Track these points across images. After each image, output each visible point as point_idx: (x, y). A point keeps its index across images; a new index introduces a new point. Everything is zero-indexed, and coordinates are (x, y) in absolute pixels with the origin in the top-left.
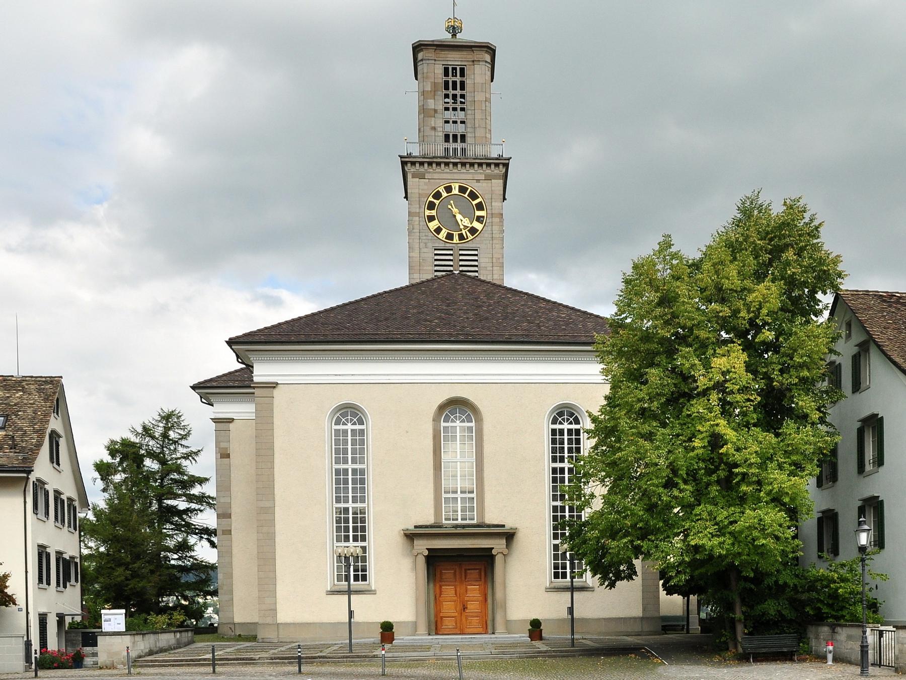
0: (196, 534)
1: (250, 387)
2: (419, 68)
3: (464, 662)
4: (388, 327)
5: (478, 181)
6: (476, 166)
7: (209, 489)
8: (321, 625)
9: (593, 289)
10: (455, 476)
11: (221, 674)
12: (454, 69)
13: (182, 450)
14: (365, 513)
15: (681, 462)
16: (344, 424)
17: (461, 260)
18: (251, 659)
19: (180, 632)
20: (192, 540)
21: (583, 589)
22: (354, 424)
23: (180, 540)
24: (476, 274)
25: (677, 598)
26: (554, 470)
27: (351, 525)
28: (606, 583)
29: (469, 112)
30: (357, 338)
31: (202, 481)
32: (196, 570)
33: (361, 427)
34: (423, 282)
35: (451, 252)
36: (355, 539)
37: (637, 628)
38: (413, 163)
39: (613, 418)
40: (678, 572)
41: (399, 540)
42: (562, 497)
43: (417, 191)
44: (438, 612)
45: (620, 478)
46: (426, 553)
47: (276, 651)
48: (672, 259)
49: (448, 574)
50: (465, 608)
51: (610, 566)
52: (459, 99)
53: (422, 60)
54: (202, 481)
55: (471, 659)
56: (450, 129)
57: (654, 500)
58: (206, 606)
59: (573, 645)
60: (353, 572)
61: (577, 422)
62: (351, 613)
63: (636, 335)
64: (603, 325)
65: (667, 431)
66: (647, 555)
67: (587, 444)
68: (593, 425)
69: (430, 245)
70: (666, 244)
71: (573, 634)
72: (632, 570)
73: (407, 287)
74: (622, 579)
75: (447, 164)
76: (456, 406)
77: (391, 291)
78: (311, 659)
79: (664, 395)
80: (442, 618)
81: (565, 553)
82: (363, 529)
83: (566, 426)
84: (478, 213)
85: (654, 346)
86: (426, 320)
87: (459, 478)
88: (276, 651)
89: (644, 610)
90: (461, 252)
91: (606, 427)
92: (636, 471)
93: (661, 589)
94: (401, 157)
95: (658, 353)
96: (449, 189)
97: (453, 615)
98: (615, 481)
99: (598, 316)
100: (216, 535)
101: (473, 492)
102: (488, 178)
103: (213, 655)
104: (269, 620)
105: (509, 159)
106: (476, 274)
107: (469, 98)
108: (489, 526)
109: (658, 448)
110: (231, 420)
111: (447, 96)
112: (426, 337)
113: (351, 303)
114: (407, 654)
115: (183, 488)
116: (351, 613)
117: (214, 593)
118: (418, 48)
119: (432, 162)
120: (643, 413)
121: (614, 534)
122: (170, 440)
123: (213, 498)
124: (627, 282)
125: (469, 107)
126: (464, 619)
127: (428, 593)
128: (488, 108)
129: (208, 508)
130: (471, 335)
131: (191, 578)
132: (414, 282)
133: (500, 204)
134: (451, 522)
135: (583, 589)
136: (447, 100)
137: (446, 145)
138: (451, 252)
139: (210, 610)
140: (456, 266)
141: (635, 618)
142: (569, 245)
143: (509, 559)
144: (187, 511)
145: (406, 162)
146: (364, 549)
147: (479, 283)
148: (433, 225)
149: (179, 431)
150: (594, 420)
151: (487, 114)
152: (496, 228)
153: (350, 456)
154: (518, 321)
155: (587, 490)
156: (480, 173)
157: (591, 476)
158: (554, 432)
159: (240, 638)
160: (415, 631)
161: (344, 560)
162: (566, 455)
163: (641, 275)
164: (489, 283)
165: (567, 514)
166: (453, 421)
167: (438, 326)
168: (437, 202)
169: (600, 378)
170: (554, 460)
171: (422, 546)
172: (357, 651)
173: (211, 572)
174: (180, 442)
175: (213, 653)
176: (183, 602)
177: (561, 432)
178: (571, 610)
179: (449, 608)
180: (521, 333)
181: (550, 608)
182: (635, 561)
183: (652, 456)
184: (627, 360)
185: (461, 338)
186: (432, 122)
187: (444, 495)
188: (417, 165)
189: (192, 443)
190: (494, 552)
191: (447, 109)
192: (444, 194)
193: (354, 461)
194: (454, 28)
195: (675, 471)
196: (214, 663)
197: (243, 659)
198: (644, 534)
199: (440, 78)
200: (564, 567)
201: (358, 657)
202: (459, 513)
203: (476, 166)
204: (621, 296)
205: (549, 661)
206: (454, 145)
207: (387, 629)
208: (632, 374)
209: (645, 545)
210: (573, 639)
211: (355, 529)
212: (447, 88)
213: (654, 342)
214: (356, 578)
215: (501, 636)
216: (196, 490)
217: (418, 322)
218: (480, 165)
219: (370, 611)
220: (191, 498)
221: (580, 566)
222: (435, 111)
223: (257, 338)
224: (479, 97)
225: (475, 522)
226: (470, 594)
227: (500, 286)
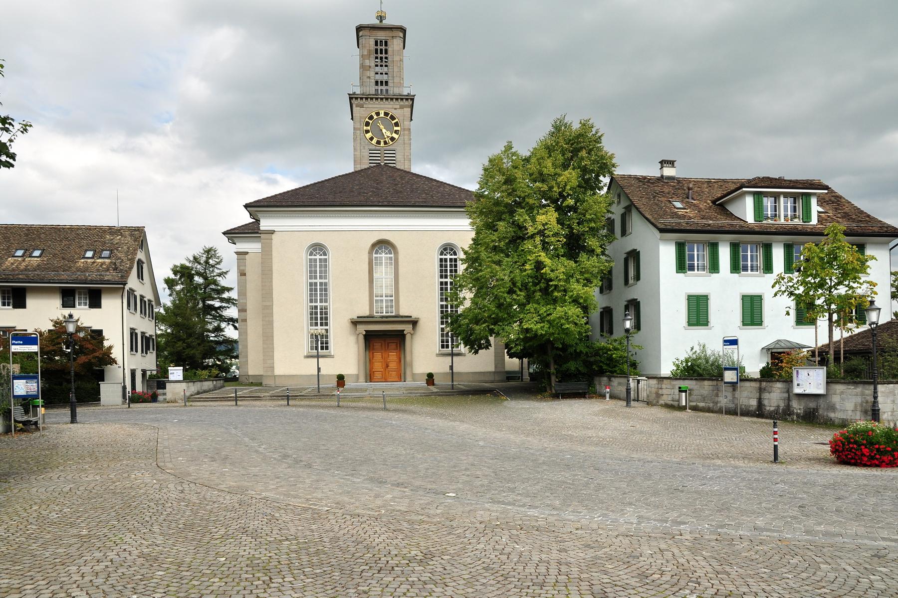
3: (387, 399)
7: (234, 295)
8: (301, 376)
11: (240, 406)
12: (381, 42)
13: (217, 271)
15: (518, 278)
20: (223, 325)
21: (459, 354)
25: (516, 360)
26: (441, 283)
31: (229, 290)
36: (322, 325)
37: (491, 378)
38: (356, 98)
39: (477, 252)
40: (516, 345)
41: (347, 325)
42: (446, 300)
45: (481, 288)
49: (377, 345)
50: (387, 366)
54: (229, 290)
57: (502, 301)
58: (231, 365)
60: (320, 344)
61: (455, 254)
62: (319, 369)
64: (471, 196)
65: (509, 259)
66: (498, 334)
67: (461, 268)
69: (367, 147)
70: (509, 147)
75: (377, 99)
76: (382, 244)
78: (295, 397)
82: (326, 319)
83: (448, 257)
84: (396, 128)
89: (496, 367)
96: (378, 114)
102: (402, 107)
104: (269, 373)
107: (390, 59)
108: (402, 317)
109: (504, 270)
111: (377, 58)
116: (319, 369)
117: (237, 357)
118: (359, 29)
120: (495, 249)
124: (485, 170)
131: (223, 348)
135: (459, 354)
139: (234, 367)
141: (490, 372)
143: (414, 337)
146: (327, 330)
148: (369, 135)
150: (466, 253)
155: (461, 295)
156: (396, 104)
157: (464, 286)
158: (441, 260)
159: (252, 384)
167: (371, 196)
170: (441, 277)
171: (362, 329)
172: (322, 392)
177: (446, 260)
178: (451, 367)
179: (378, 366)
181: (439, 366)
183: (500, 275)
186: (368, 73)
189: (223, 267)
191: (377, 66)
192: (375, 117)
193: (321, 277)
195: (514, 284)
196: (236, 399)
198: (496, 322)
200: (447, 342)
205: (438, 398)
206: (381, 87)
207: (341, 379)
208: (488, 225)
211: (321, 319)
212: (377, 53)
214: (322, 348)
215: (409, 383)
216: (226, 295)
218: (397, 99)
219: (330, 368)
220: (222, 300)
221: (457, 341)
223: (262, 204)
224: (396, 58)
226: (391, 358)
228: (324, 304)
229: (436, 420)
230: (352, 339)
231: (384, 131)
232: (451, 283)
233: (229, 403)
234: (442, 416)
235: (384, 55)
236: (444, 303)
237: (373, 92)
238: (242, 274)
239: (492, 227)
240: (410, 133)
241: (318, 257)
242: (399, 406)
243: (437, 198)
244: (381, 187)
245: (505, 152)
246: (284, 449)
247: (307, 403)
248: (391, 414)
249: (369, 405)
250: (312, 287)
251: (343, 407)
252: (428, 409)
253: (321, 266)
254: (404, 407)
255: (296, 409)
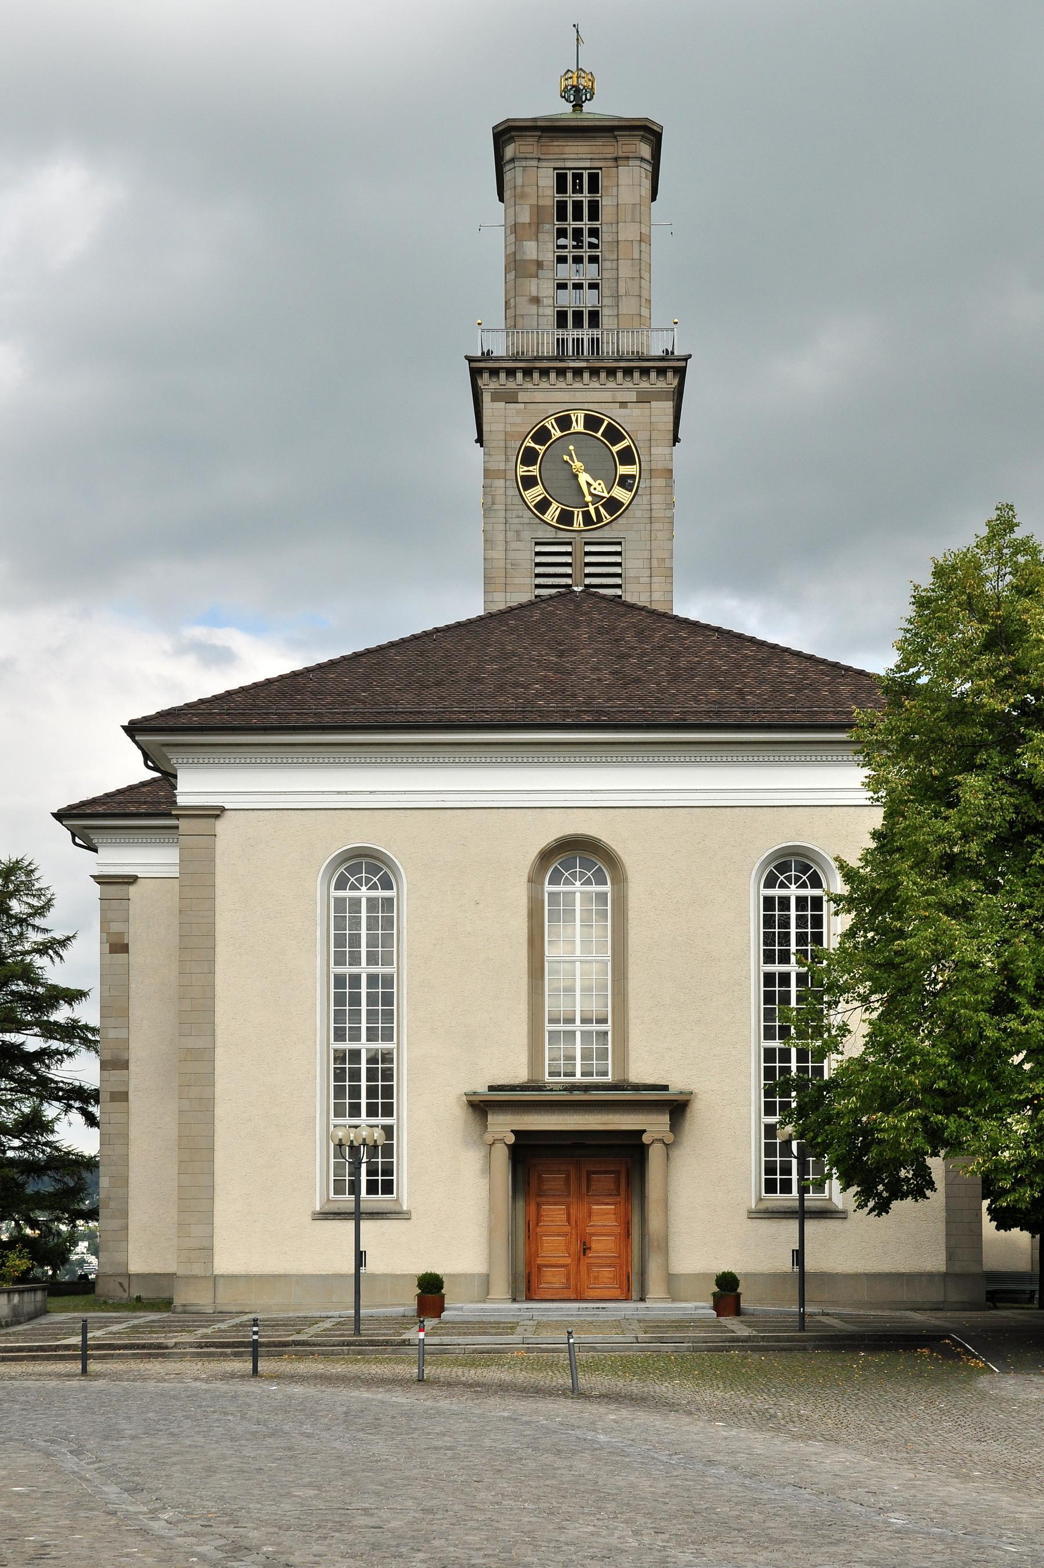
0: (58, 1099)
1: (168, 815)
2: (508, 177)
3: (582, 1356)
4: (442, 698)
5: (623, 404)
6: (620, 375)
7: (87, 1012)
8: (302, 1279)
9: (852, 621)
10: (570, 990)
11: (98, 1376)
12: (577, 177)
13: (34, 937)
14: (392, 1062)
15: (1025, 963)
16: (353, 887)
17: (588, 554)
18: (160, 1346)
19: (21, 1292)
20: (51, 1110)
21: (826, 1213)
22: (374, 887)
23: (27, 1110)
24: (618, 592)
25: (1020, 1237)
26: (769, 979)
27: (364, 1083)
28: (871, 1204)
29: (607, 265)
30: (381, 720)
31: (73, 996)
32: (57, 1169)
33: (387, 894)
34: (511, 609)
35: (569, 549)
36: (372, 1111)
37: (935, 1295)
39: (888, 875)
40: (1018, 1182)
41: (457, 1114)
42: (784, 1033)
43: (501, 427)
44: (531, 1257)
45: (904, 991)
46: (511, 1139)
47: (209, 1331)
48: (1015, 554)
49: (554, 1181)
50: (586, 1249)
51: (879, 1170)
52: (587, 239)
53: (512, 160)
54: (73, 996)
55: (595, 1349)
56: (568, 299)
57: (969, 1035)
58: (73, 1239)
59: (802, 1328)
60: (367, 1175)
61: (816, 882)
62: (360, 1258)
63: (936, 709)
64: (871, 690)
65: (996, 899)
66: (955, 1146)
67: (837, 925)
68: (848, 887)
69: (527, 535)
70: (1003, 525)
71: (802, 1304)
72: (923, 1177)
73: (480, 618)
74: (903, 1196)
75: (561, 372)
76: (576, 853)
77: (448, 628)
78: (279, 1348)
79: (993, 827)
80: (540, 1267)
81: (787, 1143)
82: (388, 1092)
83: (793, 892)
84: (623, 470)
85: (974, 732)
86: (516, 685)
87: (578, 993)
88: (209, 1331)
89: (950, 1257)
90: (588, 549)
91: (874, 891)
92: (935, 981)
93: (986, 1217)
94: (470, 359)
95: (984, 745)
96: (564, 422)
97: (562, 1261)
98: (891, 999)
99: (861, 673)
100: (97, 1102)
101: (604, 1021)
102: (644, 398)
103: (85, 1339)
104: (197, 1270)
105: (686, 359)
106: (618, 592)
107: (606, 236)
108: (637, 1088)
109: (977, 935)
110: (132, 880)
111: (562, 233)
112: (517, 718)
113: (368, 651)
114: (469, 1339)
115: (35, 1010)
116: (360, 1258)
117: (92, 1214)
118: (505, 134)
119: (530, 368)
120: (950, 864)
121: (886, 1099)
122: (10, 916)
123: (94, 1030)
124: (922, 603)
125: (607, 255)
126: (583, 1270)
127: (514, 1218)
128: (644, 257)
129: (83, 1049)
130: (606, 713)
131: (46, 1185)
132: (495, 608)
133: (667, 451)
134: (562, 1079)
135: (826, 1213)
136: (562, 241)
137: (560, 333)
138: (569, 549)
139: (82, 1246)
140: (578, 576)
141: (931, 1276)
142: (802, 546)
143: (677, 1154)
144: (42, 1054)
145: (480, 369)
146: (388, 1130)
147: (622, 609)
148: (534, 495)
149: (30, 900)
150: (850, 875)
151: (642, 267)
152: (657, 498)
153: (364, 950)
154: (699, 685)
155: (835, 1018)
156: (627, 388)
157: (844, 990)
158: (769, 902)
159: (139, 1304)
160: (485, 1294)
161: (350, 1152)
162: (793, 948)
163: (950, 588)
164: (643, 608)
165: (794, 1065)
166: (568, 882)
167: (540, 695)
168: (541, 449)
169: (864, 796)
170: (769, 958)
171: (504, 1126)
172: (368, 1331)
173: (85, 1174)
174: (31, 921)
175: (84, 1333)
176: (28, 1231)
177: (784, 902)
178: (799, 1256)
179: (554, 1247)
180: (705, 707)
181: (758, 1252)
182: (930, 1161)
183: (967, 950)
184: (919, 758)
185: (586, 718)
186: (532, 287)
187: (548, 1027)
188: (503, 375)
189: (55, 924)
190: (646, 1139)
191: (562, 260)
192: (556, 433)
193: (372, 959)
194: (577, 90)
195: (1012, 982)
196: (84, 1354)
197: (143, 1347)
198: (951, 1100)
199: (549, 196)
200: (786, 1170)
201: (372, 1343)
202: (578, 1062)
203: (620, 375)
204: (908, 631)
205: (754, 1358)
206: (577, 333)
207: (431, 1290)
208: (929, 787)
209: (952, 1124)
210: (802, 1315)
211: (372, 1092)
212: (562, 216)
213: (975, 724)
214: (372, 1188)
215: (658, 1305)
216: (61, 1015)
217: (501, 687)
219: (398, 1252)
220: (50, 1030)
221: (819, 1168)
222: (539, 264)
223: (183, 721)
224: (628, 232)
225: (609, 1079)
226: (596, 1221)
227: (665, 615)
228: (380, 1045)
229: (743, 1433)
230: (471, 1160)
231: (584, 478)
232: (801, 979)
233: (61, 1367)
234: (765, 1420)
235: (585, 224)
236: (777, 1044)
237: (548, 348)
238: (117, 946)
239: (941, 794)
240: (670, 486)
241: (364, 893)
242: (620, 1384)
243: (770, 700)
244: (579, 661)
245: (990, 540)
246: (235, 1522)
247: (319, 1367)
248: (593, 1409)
249: (521, 1377)
250: (345, 992)
251: (435, 1382)
252: (714, 1395)
253: (372, 924)
254: (636, 1386)
255: (278, 1390)
